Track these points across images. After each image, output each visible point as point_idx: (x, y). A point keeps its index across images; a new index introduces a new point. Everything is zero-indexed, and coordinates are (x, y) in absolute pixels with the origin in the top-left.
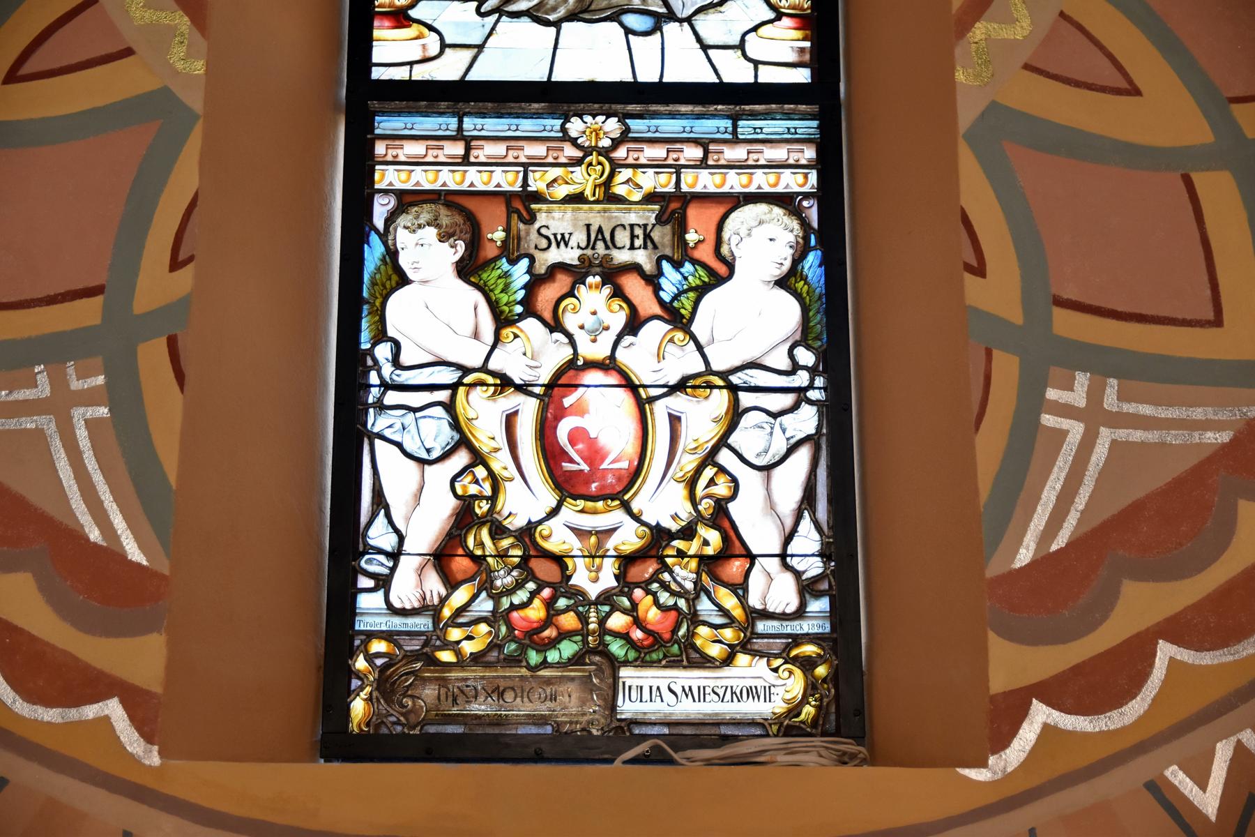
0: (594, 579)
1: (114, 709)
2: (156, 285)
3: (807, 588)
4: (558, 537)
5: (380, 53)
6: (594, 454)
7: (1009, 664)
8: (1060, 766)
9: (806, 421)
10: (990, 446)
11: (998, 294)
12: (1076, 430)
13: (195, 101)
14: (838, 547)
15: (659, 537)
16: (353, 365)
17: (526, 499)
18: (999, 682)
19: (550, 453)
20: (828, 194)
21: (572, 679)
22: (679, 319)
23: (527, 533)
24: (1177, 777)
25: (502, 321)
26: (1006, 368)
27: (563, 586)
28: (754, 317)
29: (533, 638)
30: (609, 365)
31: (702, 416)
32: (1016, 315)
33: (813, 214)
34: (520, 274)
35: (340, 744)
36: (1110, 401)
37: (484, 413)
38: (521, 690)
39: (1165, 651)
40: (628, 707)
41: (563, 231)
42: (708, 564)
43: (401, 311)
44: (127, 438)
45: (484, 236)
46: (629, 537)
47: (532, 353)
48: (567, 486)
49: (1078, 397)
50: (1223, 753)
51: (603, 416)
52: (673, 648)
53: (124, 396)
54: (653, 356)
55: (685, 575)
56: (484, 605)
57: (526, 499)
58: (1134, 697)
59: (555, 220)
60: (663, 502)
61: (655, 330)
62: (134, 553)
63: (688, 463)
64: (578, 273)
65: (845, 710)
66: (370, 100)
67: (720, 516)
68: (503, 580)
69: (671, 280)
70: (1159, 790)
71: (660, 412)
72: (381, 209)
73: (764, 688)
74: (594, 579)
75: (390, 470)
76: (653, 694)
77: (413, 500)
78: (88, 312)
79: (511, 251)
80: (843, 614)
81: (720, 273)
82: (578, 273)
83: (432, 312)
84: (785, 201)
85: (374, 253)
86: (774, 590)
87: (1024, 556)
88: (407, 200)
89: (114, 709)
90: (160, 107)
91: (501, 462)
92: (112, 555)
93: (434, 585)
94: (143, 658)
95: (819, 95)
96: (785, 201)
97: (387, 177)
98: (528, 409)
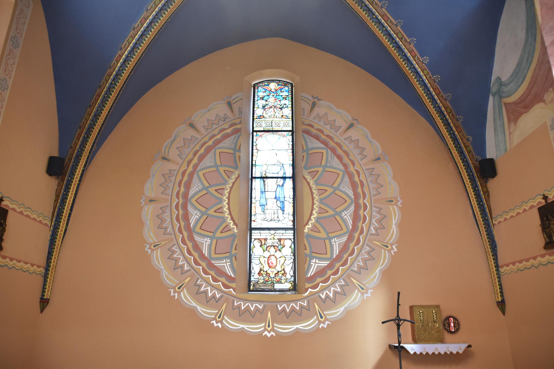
0: (272, 275)
1: (231, 289)
2: (234, 252)
3: (292, 276)
4: (269, 272)
5: (252, 225)
6: (272, 264)
7: (307, 285)
8: (311, 294)
9: (292, 260)
10: (306, 266)
11: (308, 252)
12: (314, 264)
13: (237, 234)
14: (294, 273)
15: (278, 272)
16: (250, 255)
17: (266, 268)
18: (306, 287)
19: (268, 264)
20: (294, 239)
21: (202, 184)
22: (280, 251)
23: (266, 271)
24: (321, 295)
25: (264, 251)
26: (308, 258)
27: (269, 276)
28: (287, 251)
29: (267, 281)
30: (274, 255)
31: (282, 260)
32: (309, 254)
33: (293, 240)
34: (265, 246)
35: (250, 291)
36: (317, 261)
37: (262, 260)
38: (266, 286)
39: (321, 284)
40: (275, 288)
41: (269, 242)
42: (283, 274)
43: (254, 250)
44: (232, 266)
45: (262, 242)
46: (276, 272)
47: (267, 254)
48: (270, 267)
49: (314, 261)
50: (325, 293)
51: (273, 260)
52: (279, 282)
53: (231, 262)
54: (278, 254)
55: (280, 275)
56: (262, 278)
57: (266, 268)
58: (394, 178)
59: (268, 241)
60: (279, 268)
61: (278, 252)
62: (233, 276)
63: (281, 265)
64: (271, 246)
65: (295, 288)
66: (251, 229)
67: (284, 270)
68: (264, 276)
69: (279, 247)
70: (319, 296)
71: (278, 260)
72: (253, 240)
73: (288, 286)
74: (272, 275)
75: (253, 265)
76: (277, 286)
77: (256, 268)
78: (228, 254)
79: (265, 244)
80: (295, 279)
81: (284, 246)
82: (271, 246)
83: (257, 250)
84: (290, 239)
85: (252, 244)
86: (288, 276)
87: (309, 276)
88: (255, 239)
89: (231, 289)
90: (234, 235)
91: (264, 265)
92: (231, 276)
93: (258, 276)
94: (233, 285)
95: (293, 229)
96: (290, 239)
97: (253, 237)
98: (266, 260)
